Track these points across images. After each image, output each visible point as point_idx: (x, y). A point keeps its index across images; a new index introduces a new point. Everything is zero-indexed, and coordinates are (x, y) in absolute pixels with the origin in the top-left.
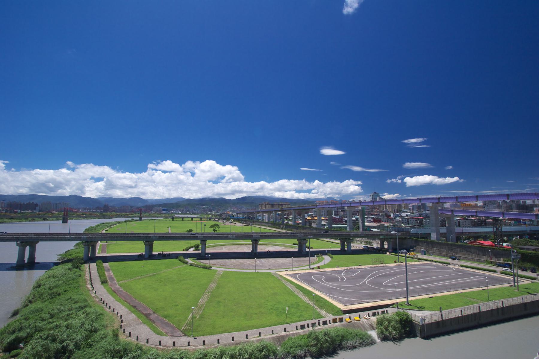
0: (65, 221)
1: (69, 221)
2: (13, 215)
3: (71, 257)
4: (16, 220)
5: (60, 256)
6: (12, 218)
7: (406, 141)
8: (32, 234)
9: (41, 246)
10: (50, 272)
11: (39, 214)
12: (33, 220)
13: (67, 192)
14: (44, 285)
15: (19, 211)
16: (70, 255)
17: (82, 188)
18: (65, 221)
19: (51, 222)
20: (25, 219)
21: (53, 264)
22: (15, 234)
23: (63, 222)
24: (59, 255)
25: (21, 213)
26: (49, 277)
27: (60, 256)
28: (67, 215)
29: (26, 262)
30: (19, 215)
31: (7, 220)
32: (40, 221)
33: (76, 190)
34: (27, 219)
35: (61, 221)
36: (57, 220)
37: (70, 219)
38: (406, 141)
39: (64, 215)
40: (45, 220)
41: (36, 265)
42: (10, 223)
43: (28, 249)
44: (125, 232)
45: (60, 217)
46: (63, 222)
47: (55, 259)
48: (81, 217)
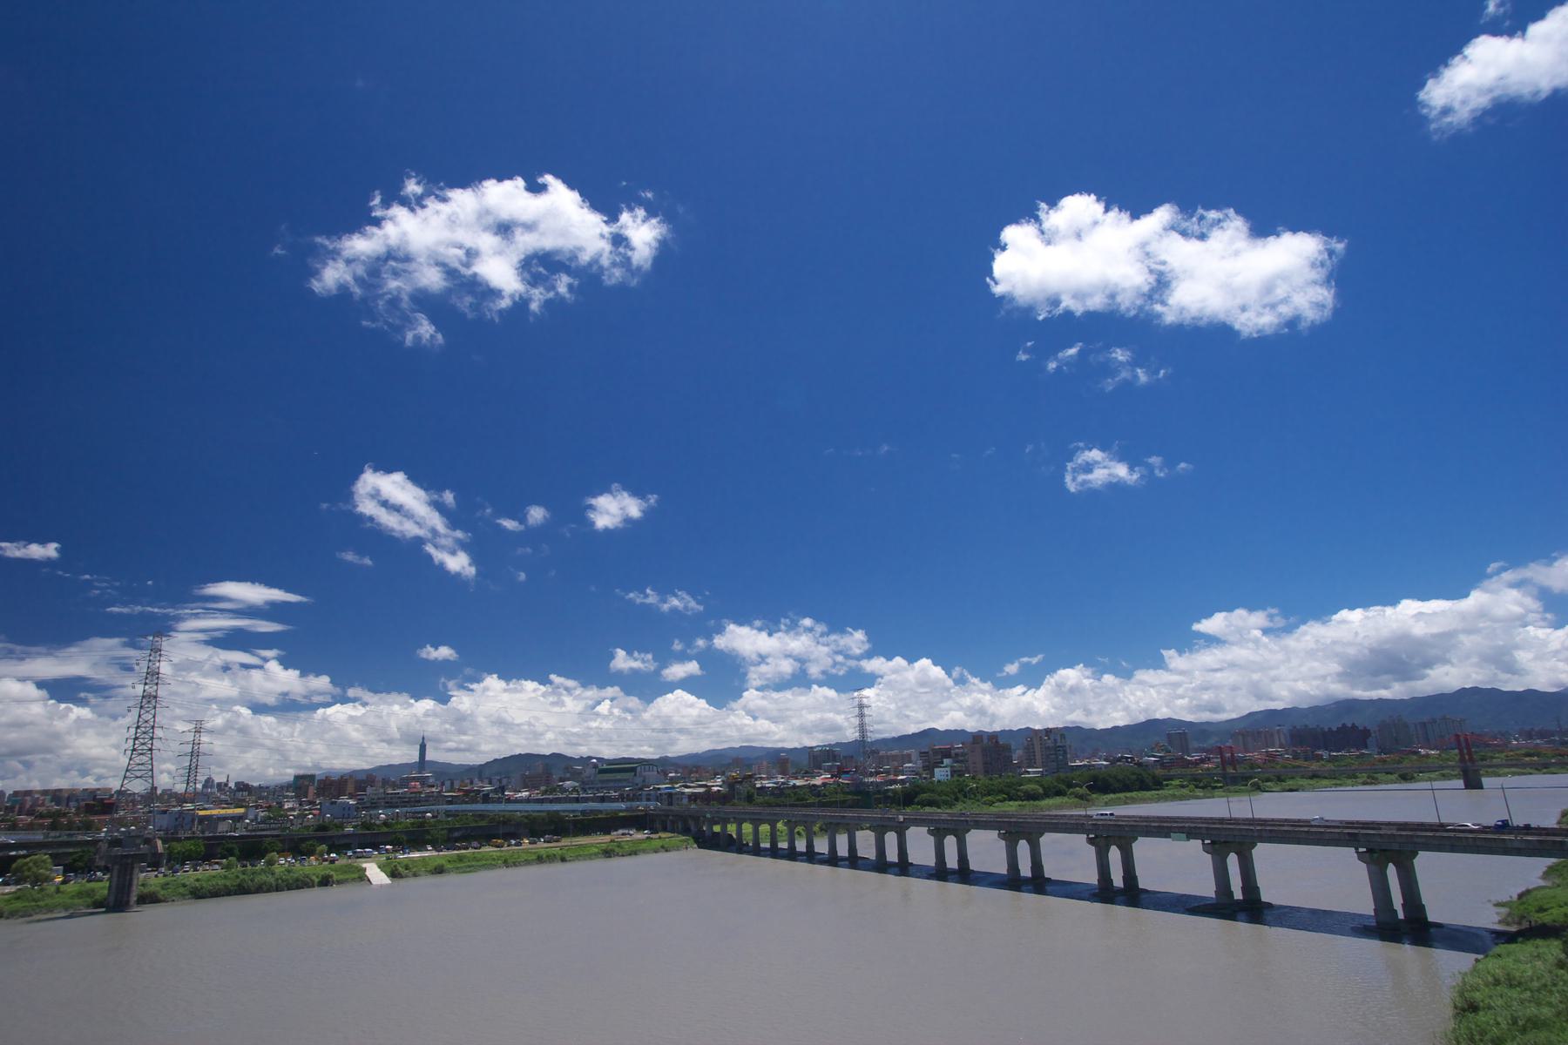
0: (1473, 783)
1: (1485, 781)
2: (1315, 766)
3: (1546, 918)
4: (1325, 782)
5: (1504, 910)
6: (1314, 776)
7: (304, 599)
8: (1389, 824)
9: (1144, 848)
10: (1493, 966)
11: (1384, 761)
12: (1372, 780)
13: (1448, 677)
14: (1490, 1008)
15: (1325, 754)
16: (1541, 910)
17: (1501, 659)
18: (1473, 783)
19: (1437, 784)
20: (1349, 777)
21: (1488, 938)
22: (1350, 824)
23: (1469, 786)
24: (1498, 905)
25: (1332, 759)
26: (1497, 982)
27: (1504, 910)
28: (1471, 759)
29: (1401, 916)
30: (1330, 766)
31: (1304, 782)
32: (1393, 782)
33: (1343, 677)
34: (1352, 776)
35: (1460, 783)
36: (1445, 777)
37: (1488, 775)
38: (304, 599)
39: (1462, 760)
40: (1405, 778)
41: (1143, 896)
42: (1313, 788)
43: (1391, 870)
44: (1227, 815)
45: (1453, 768)
46: (1469, 786)
47: (1489, 919)
48: (1524, 766)
